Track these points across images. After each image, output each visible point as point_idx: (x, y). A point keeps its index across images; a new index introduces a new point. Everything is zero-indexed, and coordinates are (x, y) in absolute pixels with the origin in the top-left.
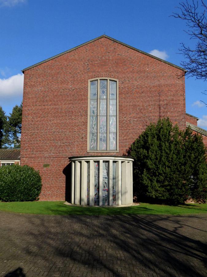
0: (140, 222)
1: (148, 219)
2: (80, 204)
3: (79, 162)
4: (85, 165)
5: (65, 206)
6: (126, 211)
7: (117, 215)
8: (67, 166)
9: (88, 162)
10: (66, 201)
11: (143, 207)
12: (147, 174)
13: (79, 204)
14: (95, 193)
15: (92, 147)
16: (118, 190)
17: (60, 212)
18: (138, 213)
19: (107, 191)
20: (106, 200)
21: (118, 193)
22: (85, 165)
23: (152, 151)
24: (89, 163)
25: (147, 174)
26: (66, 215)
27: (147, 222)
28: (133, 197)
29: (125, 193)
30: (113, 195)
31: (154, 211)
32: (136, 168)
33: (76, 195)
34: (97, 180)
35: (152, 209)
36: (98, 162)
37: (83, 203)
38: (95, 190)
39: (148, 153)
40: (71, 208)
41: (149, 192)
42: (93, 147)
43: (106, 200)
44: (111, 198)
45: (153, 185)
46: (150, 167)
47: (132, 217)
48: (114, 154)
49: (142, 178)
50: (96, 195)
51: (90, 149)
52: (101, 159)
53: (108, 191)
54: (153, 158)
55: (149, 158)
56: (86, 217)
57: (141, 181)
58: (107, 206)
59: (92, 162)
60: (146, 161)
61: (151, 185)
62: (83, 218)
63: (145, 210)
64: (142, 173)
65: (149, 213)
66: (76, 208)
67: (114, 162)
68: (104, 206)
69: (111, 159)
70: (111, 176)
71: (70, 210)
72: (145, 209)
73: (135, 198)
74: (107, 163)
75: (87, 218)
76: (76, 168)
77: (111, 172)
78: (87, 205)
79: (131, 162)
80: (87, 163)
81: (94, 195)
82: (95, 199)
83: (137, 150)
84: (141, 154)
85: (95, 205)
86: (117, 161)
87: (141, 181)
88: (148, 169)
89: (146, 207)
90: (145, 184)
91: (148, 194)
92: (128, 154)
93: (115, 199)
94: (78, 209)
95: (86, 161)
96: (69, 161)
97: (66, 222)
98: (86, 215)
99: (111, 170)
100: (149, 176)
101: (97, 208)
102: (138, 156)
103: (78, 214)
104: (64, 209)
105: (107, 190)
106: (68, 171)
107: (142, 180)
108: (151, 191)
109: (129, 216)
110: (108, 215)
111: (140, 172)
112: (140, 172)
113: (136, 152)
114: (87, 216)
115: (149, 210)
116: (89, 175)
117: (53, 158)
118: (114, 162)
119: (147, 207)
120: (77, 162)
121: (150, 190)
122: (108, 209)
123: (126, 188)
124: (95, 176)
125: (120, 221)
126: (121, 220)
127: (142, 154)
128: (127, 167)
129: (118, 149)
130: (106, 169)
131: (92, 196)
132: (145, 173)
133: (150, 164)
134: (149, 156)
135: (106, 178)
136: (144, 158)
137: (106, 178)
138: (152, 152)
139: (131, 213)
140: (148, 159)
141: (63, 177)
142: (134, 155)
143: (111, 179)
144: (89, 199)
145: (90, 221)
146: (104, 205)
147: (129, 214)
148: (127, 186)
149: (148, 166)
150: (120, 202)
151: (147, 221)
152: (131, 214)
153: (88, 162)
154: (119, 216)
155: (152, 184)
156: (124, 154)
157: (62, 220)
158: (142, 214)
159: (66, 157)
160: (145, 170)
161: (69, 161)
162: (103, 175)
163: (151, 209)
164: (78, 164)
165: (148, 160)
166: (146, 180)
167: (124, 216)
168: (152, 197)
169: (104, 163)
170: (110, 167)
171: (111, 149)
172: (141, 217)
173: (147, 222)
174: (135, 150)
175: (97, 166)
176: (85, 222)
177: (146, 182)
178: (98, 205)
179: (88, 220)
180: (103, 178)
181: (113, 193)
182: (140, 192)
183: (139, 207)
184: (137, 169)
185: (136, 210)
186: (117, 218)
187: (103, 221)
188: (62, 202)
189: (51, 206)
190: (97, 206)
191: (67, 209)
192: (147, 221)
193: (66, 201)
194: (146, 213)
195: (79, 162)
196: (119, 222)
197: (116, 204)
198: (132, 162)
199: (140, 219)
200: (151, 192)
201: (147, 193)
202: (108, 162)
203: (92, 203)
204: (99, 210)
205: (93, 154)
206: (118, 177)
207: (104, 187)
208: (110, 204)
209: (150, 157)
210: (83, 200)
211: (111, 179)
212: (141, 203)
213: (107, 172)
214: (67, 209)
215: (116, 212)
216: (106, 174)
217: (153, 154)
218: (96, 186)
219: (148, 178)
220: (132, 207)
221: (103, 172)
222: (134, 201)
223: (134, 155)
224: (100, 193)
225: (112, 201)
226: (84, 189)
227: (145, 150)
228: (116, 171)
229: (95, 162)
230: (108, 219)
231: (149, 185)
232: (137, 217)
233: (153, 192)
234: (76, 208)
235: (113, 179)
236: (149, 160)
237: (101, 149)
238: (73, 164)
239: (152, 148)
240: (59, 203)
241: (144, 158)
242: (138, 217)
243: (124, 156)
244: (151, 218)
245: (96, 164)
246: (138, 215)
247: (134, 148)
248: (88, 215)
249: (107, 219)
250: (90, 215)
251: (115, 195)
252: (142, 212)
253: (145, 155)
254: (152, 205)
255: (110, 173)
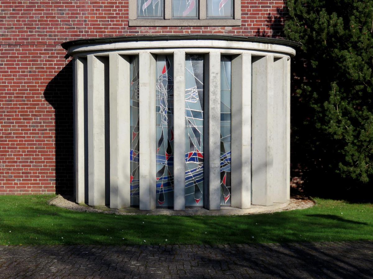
0: (325, 271)
1: (355, 259)
2: (108, 203)
3: (100, 58)
4: (121, 69)
5: (55, 212)
6: (268, 228)
7: (240, 246)
8: (61, 74)
9: (132, 59)
10: (57, 194)
11: (326, 213)
12: (343, 99)
13: (103, 203)
14: (160, 168)
15: (145, 6)
16: (241, 156)
17: (32, 236)
18: (316, 234)
19: (200, 160)
20: (197, 190)
21: (240, 166)
22: (121, 69)
23: (363, 20)
24: (135, 62)
25: (343, 99)
26: (52, 244)
27: (352, 269)
28: (291, 180)
29: (266, 165)
30: (222, 174)
31: (367, 228)
32: (301, 81)
33: (93, 173)
34: (166, 123)
35: (361, 220)
36: (169, 58)
37: (115, 202)
38: (159, 157)
39: (347, 26)
40: (74, 219)
41: (347, 164)
42: (150, 7)
43: (197, 190)
44: (215, 184)
45: (362, 138)
46: (355, 74)
47: (296, 251)
48: (224, 32)
49: (325, 115)
50: (161, 172)
51: (141, 15)
52: (179, 50)
53: (205, 159)
54: (364, 45)
55: (350, 45)
56: (124, 252)
57: (318, 125)
58: (202, 212)
59: (145, 58)
60: (340, 54)
61: (357, 137)
62: (115, 258)
63: (337, 226)
64: (325, 96)
65: (353, 234)
66: (93, 218)
67: (227, 58)
68: (191, 212)
69: (215, 49)
70: (215, 108)
71: (68, 225)
72: (335, 222)
73: (297, 183)
74: (201, 63)
75: (132, 256)
76: (91, 77)
77: (214, 93)
78: (131, 206)
79: (286, 57)
80: (128, 64)
81: (154, 172)
82: (158, 186)
83: (305, 15)
84: (321, 30)
85: (158, 207)
86: (238, 55)
87: (318, 125)
88: (347, 85)
89: (338, 214)
90: (335, 133)
91: (345, 168)
92: (277, 31)
93: (228, 187)
94: (99, 223)
95: (124, 56)
96: (67, 57)
97: (49, 271)
98: (127, 245)
99: (216, 87)
100: (350, 108)
101: (166, 217)
102: (311, 37)
103: (97, 243)
104: (47, 222)
105: (199, 155)
106: (61, 93)
107: (325, 122)
108: (355, 158)
109: (283, 246)
110: (207, 243)
111: (315, 95)
112: (315, 95)
113: (304, 25)
114: (128, 249)
115: (350, 225)
116: (135, 105)
117: (10, 45)
118: (227, 58)
119: (342, 214)
120: (91, 58)
121: (353, 155)
122: (205, 223)
123: (267, 149)
124: (158, 109)
125: (251, 267)
126: (255, 264)
127: (326, 31)
128: (271, 77)
129: (238, 14)
130: (197, 82)
131: (148, 177)
132: (335, 95)
133: (354, 66)
134: (351, 36)
135: (196, 114)
136: (331, 45)
137: (196, 114)
138: (360, 22)
139: (291, 237)
140: (347, 48)
141: (47, 113)
142: (297, 35)
143: (214, 118)
144: (138, 186)
145: (142, 268)
146: (191, 207)
147: (284, 242)
148: (270, 143)
149: (345, 72)
150: (246, 197)
151: (351, 265)
152: (292, 241)
153: (132, 59)
154: (246, 246)
155: (359, 133)
156: (258, 32)
157: (37, 266)
158: (328, 241)
159: (56, 44)
160: (334, 85)
161: (67, 57)
162: (187, 104)
163: (356, 220)
164: (97, 67)
165: (345, 52)
166: (339, 122)
167: (263, 246)
168: (357, 181)
169: (190, 62)
170: (212, 76)
171: (213, 13)
172: (327, 252)
173: (352, 269)
174: (300, 18)
175: (164, 72)
176: (123, 271)
177: (338, 128)
178: (171, 207)
179: (134, 264)
180: (188, 113)
181: (222, 165)
182: (316, 160)
183: (313, 212)
184: (305, 84)
185: (305, 224)
186: (244, 256)
187: (187, 267)
188: (45, 197)
189: (5, 211)
190: (166, 212)
191: (58, 221)
192: (351, 265)
193: (57, 194)
194: (343, 236)
195: (98, 57)
196: (250, 271)
197: (233, 202)
198: (289, 57)
199: (326, 258)
200: (354, 162)
201: (340, 164)
202: (204, 57)
203: (147, 201)
204: (172, 224)
205: (151, 32)
206: (240, 110)
207: (192, 145)
208: (213, 204)
209: (355, 39)
210: (116, 190)
211: (214, 118)
212: (317, 200)
213: (199, 92)
214: (58, 221)
215: (233, 234)
216: (197, 101)
217: (365, 31)
218: (160, 142)
219: (345, 113)
220: (290, 216)
221: (186, 92)
222: (294, 193)
223: (297, 35)
224: (178, 168)
225: (220, 192)
226: (122, 146)
227: (334, 15)
228: (232, 88)
229: (157, 57)
230: (206, 262)
231: (349, 138)
232: (314, 253)
233: (363, 163)
234: (93, 218)
235: (223, 117)
236: (349, 52)
237: (177, 14)
238: (80, 65)
239: (360, 9)
240: (35, 200)
241: (331, 45)
242: (316, 250)
243: (260, 38)
244: (365, 255)
245: (163, 64)
246: (318, 245)
247: (295, 9)
248: (132, 245)
249: (202, 258)
250: (139, 246)
251: (229, 174)
252: (330, 233)
253: (336, 32)
254: (356, 206)
255: (212, 97)
